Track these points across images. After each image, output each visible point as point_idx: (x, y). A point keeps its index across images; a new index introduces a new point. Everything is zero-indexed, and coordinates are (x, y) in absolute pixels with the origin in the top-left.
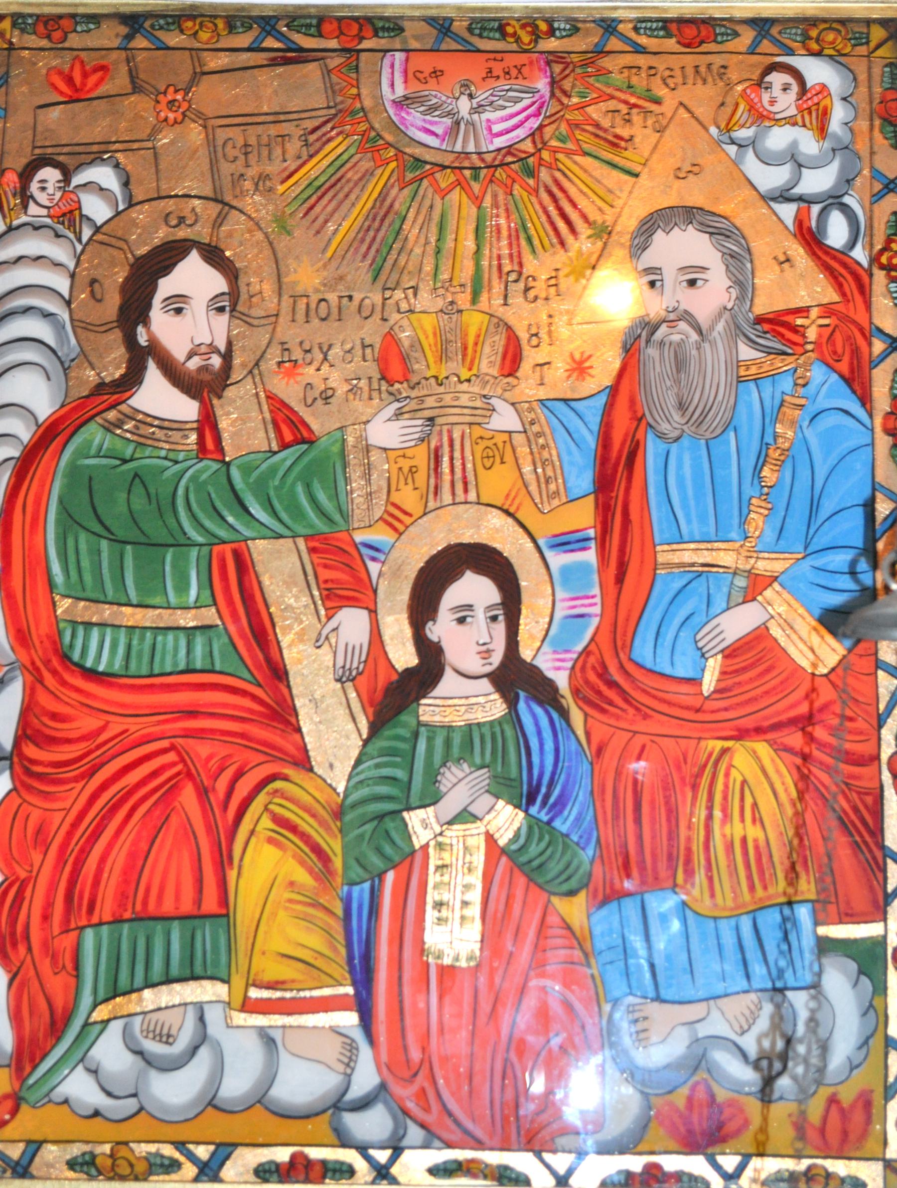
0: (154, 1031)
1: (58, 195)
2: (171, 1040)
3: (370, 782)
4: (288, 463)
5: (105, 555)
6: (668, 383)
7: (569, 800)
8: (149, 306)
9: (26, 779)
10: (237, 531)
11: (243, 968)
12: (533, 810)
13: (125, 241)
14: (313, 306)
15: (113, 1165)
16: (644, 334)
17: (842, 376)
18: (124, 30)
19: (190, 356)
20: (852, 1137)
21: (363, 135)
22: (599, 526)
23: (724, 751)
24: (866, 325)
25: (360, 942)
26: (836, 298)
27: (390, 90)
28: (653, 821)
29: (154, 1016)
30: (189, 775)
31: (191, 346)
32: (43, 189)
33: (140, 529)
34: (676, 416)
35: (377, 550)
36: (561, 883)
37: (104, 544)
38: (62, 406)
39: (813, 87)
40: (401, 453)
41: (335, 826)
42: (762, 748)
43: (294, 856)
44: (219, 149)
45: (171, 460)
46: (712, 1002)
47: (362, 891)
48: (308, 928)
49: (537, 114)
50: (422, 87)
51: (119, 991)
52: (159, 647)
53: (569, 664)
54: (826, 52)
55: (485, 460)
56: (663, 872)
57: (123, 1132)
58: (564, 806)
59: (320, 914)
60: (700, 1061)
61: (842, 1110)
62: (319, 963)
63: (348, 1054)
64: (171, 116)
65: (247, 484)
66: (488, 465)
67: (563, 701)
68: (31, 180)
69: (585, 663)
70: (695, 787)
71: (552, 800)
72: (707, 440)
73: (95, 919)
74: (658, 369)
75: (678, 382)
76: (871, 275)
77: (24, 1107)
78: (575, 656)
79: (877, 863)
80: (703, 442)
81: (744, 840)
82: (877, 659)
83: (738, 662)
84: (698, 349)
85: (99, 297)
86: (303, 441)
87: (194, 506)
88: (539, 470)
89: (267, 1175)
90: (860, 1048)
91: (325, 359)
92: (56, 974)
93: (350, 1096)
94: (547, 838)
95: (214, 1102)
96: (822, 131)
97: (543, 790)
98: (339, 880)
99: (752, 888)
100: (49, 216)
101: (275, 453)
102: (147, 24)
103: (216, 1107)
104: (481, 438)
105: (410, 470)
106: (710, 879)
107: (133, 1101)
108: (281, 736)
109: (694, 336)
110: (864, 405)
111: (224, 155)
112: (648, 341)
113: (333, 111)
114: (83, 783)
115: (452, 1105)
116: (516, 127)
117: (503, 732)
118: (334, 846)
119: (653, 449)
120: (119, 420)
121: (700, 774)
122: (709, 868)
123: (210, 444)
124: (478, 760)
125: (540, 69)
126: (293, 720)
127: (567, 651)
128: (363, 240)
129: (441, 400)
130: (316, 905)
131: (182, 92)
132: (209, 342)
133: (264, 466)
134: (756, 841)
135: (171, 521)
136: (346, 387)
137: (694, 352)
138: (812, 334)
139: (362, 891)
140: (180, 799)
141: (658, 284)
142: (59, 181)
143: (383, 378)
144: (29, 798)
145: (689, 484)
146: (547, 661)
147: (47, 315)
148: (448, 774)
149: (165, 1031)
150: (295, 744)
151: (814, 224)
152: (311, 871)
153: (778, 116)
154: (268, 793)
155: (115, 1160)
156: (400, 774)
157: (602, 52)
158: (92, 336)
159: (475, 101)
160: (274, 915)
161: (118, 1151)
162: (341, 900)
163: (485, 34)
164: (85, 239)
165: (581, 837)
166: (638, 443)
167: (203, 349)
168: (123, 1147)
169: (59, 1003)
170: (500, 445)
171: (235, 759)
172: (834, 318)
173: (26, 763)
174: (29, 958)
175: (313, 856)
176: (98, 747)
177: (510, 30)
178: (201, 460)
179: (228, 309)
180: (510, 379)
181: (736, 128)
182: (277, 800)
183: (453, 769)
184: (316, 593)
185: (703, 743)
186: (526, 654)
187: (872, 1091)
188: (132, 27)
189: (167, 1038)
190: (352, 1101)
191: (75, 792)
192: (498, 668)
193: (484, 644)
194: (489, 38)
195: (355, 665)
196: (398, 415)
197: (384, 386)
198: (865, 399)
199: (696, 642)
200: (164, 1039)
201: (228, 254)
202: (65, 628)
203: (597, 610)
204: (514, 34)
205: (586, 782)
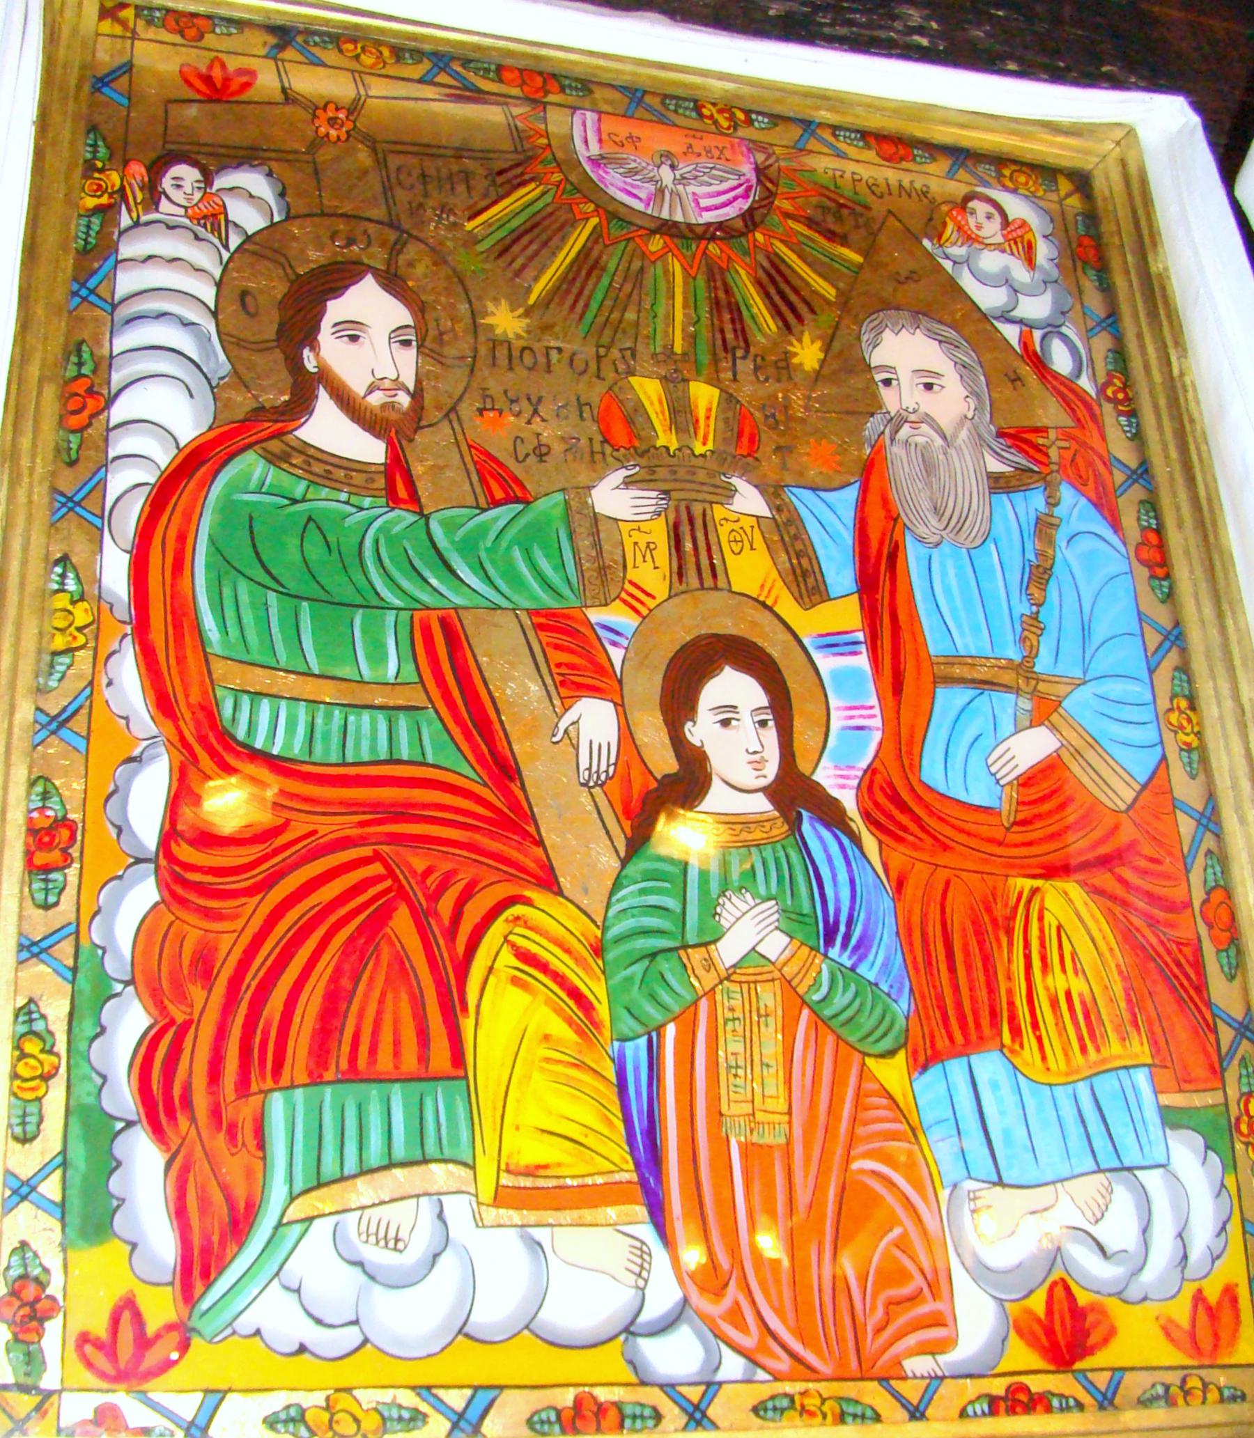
0: (377, 1234)
1: (198, 196)
2: (401, 1245)
3: (635, 911)
4: (502, 523)
5: (274, 611)
6: (920, 486)
7: (873, 940)
8: (316, 329)
9: (179, 890)
10: (441, 594)
11: (492, 1147)
12: (834, 952)
13: (285, 256)
14: (516, 354)
15: (331, 1421)
16: (887, 431)
17: (1090, 500)
18: (272, 40)
19: (370, 390)
20: (1223, 1342)
21: (558, 186)
22: (867, 629)
23: (1035, 891)
24: (1104, 453)
25: (640, 1112)
26: (1069, 422)
27: (583, 147)
28: (969, 967)
29: (375, 1213)
30: (403, 894)
31: (372, 379)
32: (179, 186)
33: (318, 582)
34: (933, 521)
35: (618, 633)
36: (877, 1041)
37: (272, 598)
38: (211, 429)
39: (1014, 220)
40: (635, 525)
41: (595, 964)
42: (1073, 888)
43: (548, 1002)
44: (393, 176)
45: (352, 505)
46: (1059, 1185)
47: (637, 1048)
48: (573, 1096)
49: (745, 196)
50: (617, 149)
51: (323, 1180)
52: (351, 729)
53: (855, 783)
54: (1021, 191)
55: (733, 544)
56: (987, 1030)
57: (346, 1374)
58: (869, 949)
59: (587, 1078)
60: (1055, 1258)
61: (1209, 1309)
62: (590, 1141)
63: (639, 1261)
64: (333, 133)
65: (453, 543)
66: (737, 550)
67: (852, 824)
68: (164, 175)
69: (872, 782)
70: (1010, 932)
71: (853, 941)
72: (968, 550)
73: (285, 1079)
74: (907, 470)
75: (929, 485)
76: (1100, 406)
77: (196, 1341)
78: (860, 774)
79: (1208, 1025)
80: (964, 551)
81: (1068, 995)
82: (1173, 798)
83: (1033, 793)
84: (945, 454)
85: (252, 310)
86: (516, 500)
87: (387, 562)
88: (795, 561)
89: (546, 1427)
90: (1218, 1235)
91: (535, 412)
92: (233, 1155)
93: (643, 1318)
94: (853, 987)
95: (466, 1329)
96: (1030, 262)
97: (842, 929)
98: (607, 1034)
99: (1083, 1049)
100: (186, 216)
101: (484, 510)
102: (300, 39)
103: (467, 1336)
104: (726, 520)
105: (648, 547)
106: (1039, 1040)
107: (355, 1329)
108: (519, 850)
109: (939, 442)
110: (1116, 532)
111: (400, 183)
112: (892, 440)
113: (521, 157)
114: (259, 897)
115: (774, 1323)
116: (724, 205)
117: (787, 856)
118: (596, 990)
119: (914, 554)
120: (283, 452)
121: (1013, 917)
122: (1035, 1026)
123: (402, 493)
124: (762, 890)
125: (743, 155)
126: (531, 829)
127: (851, 768)
128: (568, 292)
129: (675, 473)
130: (579, 1065)
131: (344, 111)
132: (394, 377)
133: (471, 524)
134: (1081, 995)
135: (359, 578)
136: (563, 447)
137: (941, 457)
138: (1053, 453)
139: (637, 1048)
140: (391, 924)
141: (894, 383)
142: (198, 181)
143: (606, 441)
144: (180, 914)
145: (955, 591)
146: (829, 777)
147: (186, 324)
148: (728, 905)
149: (392, 1234)
150: (537, 860)
151: (1038, 349)
152: (570, 1022)
153: (987, 241)
154: (507, 920)
155: (332, 1415)
156: (672, 903)
157: (801, 150)
158: (245, 354)
159: (678, 173)
160: (528, 1077)
161: (336, 1401)
162: (613, 1060)
163: (681, 111)
164: (233, 247)
165: (891, 986)
166: (897, 542)
167: (387, 384)
168: (343, 1395)
169: (240, 1195)
170: (748, 531)
171: (460, 877)
172: (1073, 443)
173: (177, 869)
174: (193, 1131)
175: (571, 1003)
176: (277, 851)
177: (705, 112)
178: (393, 509)
179: (414, 343)
180: (750, 460)
181: (948, 244)
182: (518, 930)
183: (734, 899)
184: (549, 681)
185: (1011, 881)
186: (803, 766)
187: (1237, 1285)
188: (281, 38)
189: (396, 1243)
190: (648, 1323)
191: (249, 910)
192: (773, 782)
193: (755, 753)
194: (686, 116)
195: (603, 767)
196: (628, 483)
197: (608, 449)
198: (1116, 525)
199: (988, 767)
200: (391, 1244)
201: (410, 284)
202: (224, 698)
203: (877, 722)
204: (711, 117)
205: (890, 921)
